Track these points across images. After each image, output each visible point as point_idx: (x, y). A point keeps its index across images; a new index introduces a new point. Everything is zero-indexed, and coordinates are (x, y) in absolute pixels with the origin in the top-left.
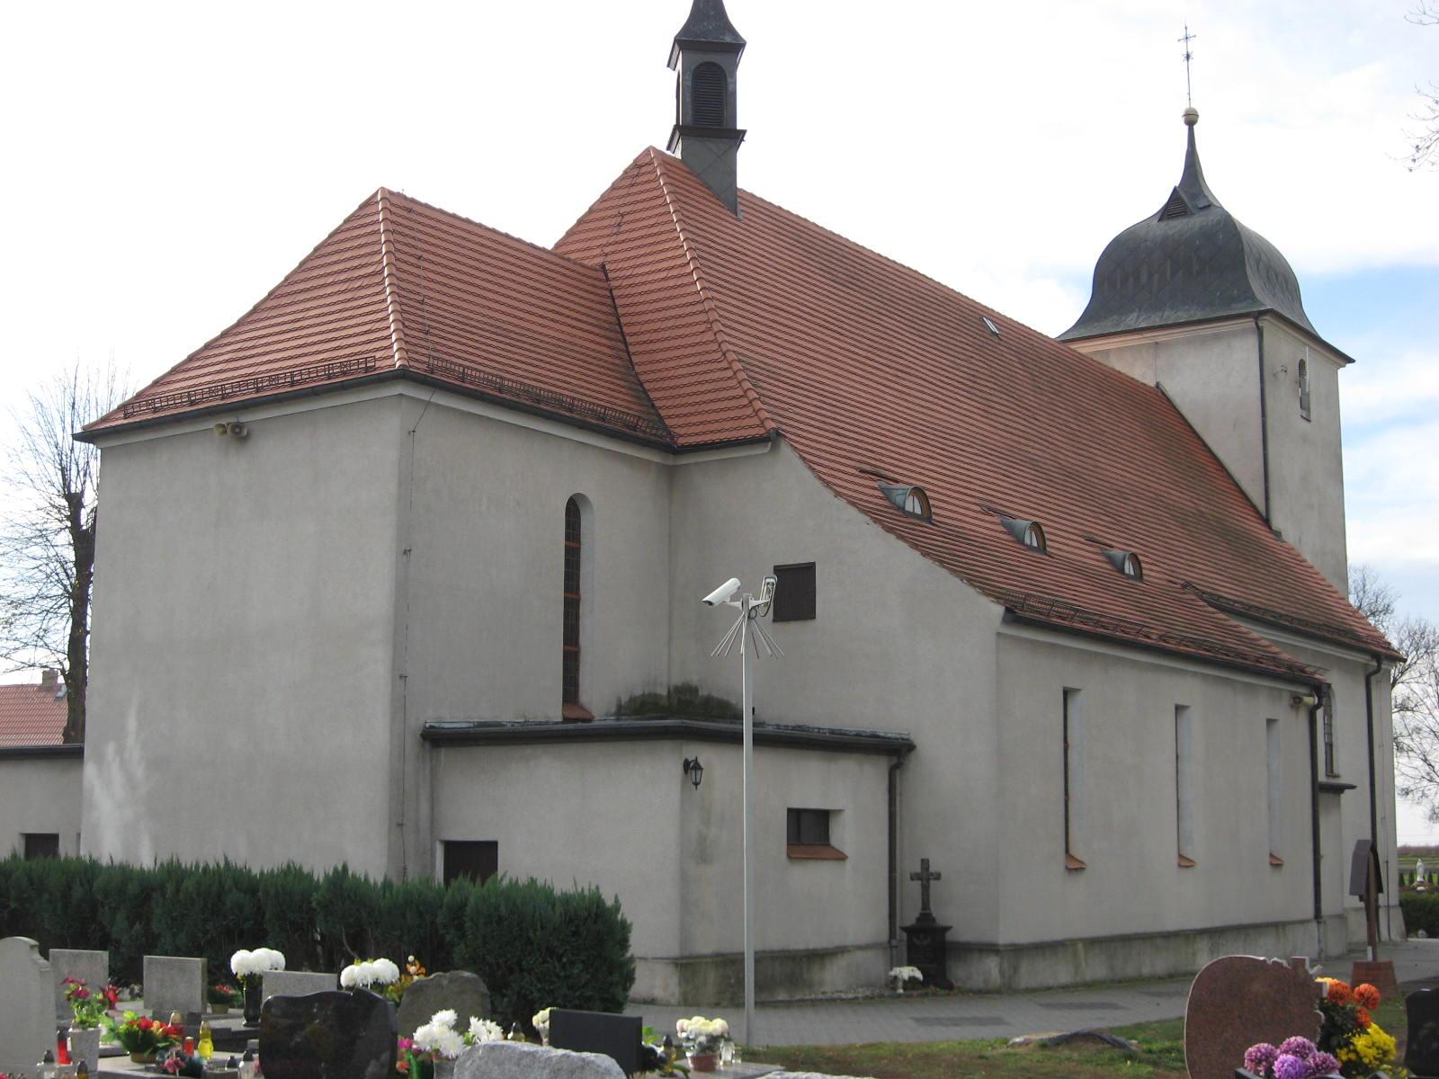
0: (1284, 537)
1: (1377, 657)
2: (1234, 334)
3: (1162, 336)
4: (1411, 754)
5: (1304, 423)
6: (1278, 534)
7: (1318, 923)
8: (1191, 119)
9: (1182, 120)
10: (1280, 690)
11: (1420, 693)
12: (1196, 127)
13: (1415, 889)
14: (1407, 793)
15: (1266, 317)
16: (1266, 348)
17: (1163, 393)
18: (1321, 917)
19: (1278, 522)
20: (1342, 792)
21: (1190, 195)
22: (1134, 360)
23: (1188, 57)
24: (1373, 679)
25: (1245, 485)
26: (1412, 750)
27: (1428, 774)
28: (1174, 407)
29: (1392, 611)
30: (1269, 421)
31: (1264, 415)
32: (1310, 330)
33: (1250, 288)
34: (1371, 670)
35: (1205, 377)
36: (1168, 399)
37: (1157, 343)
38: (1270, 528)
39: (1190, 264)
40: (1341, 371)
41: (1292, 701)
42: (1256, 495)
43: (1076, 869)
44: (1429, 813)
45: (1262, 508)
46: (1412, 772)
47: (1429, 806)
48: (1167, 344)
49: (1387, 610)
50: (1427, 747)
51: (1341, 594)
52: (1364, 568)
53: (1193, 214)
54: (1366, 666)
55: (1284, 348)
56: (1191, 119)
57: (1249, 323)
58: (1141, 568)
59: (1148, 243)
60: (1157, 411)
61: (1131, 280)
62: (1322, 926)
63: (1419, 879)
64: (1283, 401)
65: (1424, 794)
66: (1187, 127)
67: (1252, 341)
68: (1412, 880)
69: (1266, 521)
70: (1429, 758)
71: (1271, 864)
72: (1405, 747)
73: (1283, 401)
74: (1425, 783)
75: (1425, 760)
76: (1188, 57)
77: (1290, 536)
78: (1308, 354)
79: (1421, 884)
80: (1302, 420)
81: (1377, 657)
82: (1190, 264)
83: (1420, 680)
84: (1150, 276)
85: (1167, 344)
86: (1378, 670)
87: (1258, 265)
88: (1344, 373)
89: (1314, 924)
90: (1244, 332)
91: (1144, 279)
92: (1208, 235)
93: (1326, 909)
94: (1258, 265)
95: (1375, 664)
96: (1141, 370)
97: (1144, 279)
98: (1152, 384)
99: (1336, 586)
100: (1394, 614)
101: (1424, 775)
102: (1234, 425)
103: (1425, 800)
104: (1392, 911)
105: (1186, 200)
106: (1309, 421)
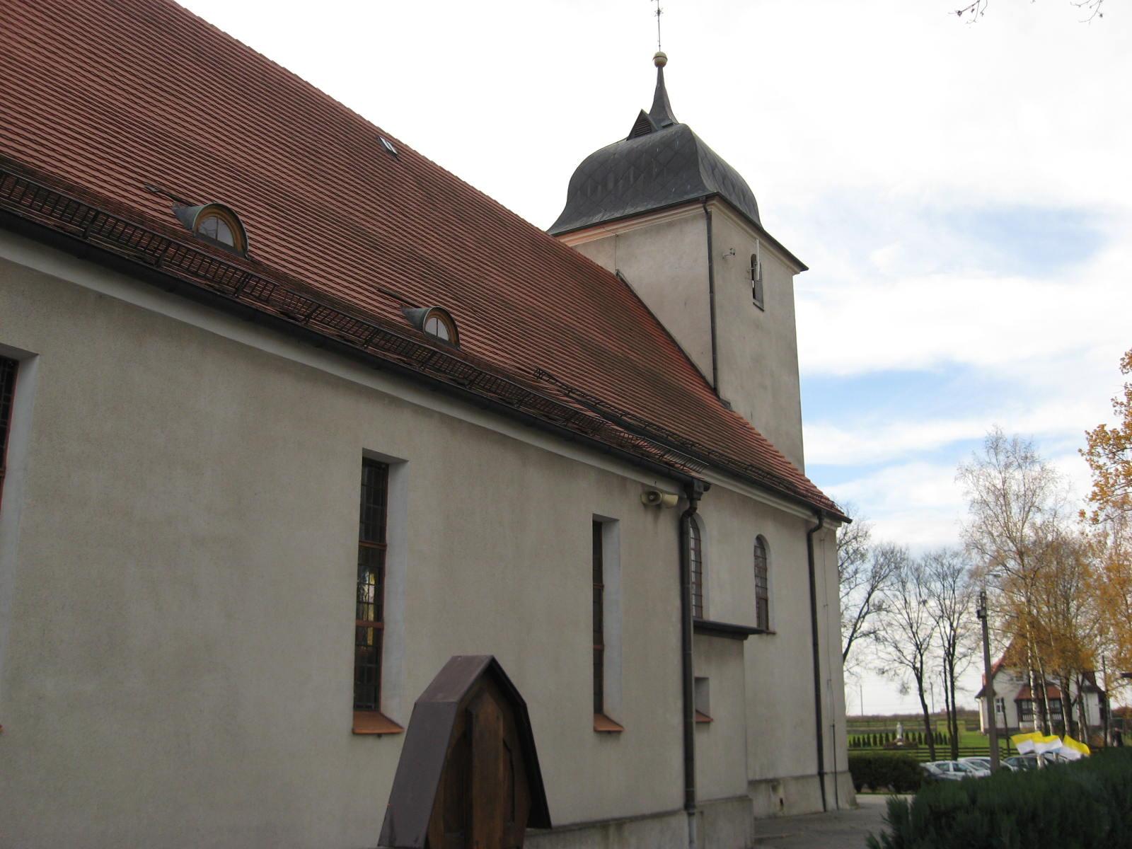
0: (734, 406)
1: (817, 512)
2: (686, 221)
3: (621, 229)
4: (886, 643)
5: (758, 311)
6: (726, 404)
7: (690, 815)
8: (660, 62)
9: (653, 63)
10: (625, 479)
11: (891, 597)
12: (664, 69)
13: (895, 744)
14: (883, 673)
15: (714, 202)
16: (714, 230)
17: (622, 280)
18: (694, 807)
19: (726, 392)
20: (746, 638)
21: (655, 120)
22: (599, 250)
23: (659, 12)
24: (815, 535)
25: (695, 358)
26: (887, 640)
27: (899, 658)
28: (632, 291)
29: (870, 536)
30: (718, 298)
31: (712, 291)
32: (757, 222)
33: (702, 182)
34: (813, 526)
35: (659, 262)
36: (627, 285)
37: (617, 236)
38: (718, 397)
39: (658, 170)
40: (796, 278)
41: (644, 499)
42: (705, 367)
43: (609, 732)
44: (900, 687)
45: (710, 378)
46: (888, 657)
47: (900, 682)
48: (625, 236)
49: (866, 535)
50: (897, 638)
51: (799, 472)
52: (848, 504)
53: (656, 131)
54: (807, 522)
55: (730, 234)
56: (660, 62)
57: (698, 210)
58: (457, 333)
59: (616, 156)
60: (616, 296)
61: (600, 187)
62: (695, 821)
63: (898, 737)
64: (734, 287)
65: (896, 674)
66: (656, 69)
67: (701, 226)
68: (894, 737)
69: (714, 390)
70: (899, 645)
71: (596, 731)
72: (881, 637)
73: (734, 287)
74: (897, 664)
75: (896, 647)
76: (659, 12)
77: (741, 408)
78: (757, 248)
79: (900, 740)
80: (755, 308)
81: (817, 512)
82: (658, 170)
83: (892, 588)
84: (616, 182)
85: (625, 236)
86: (819, 527)
87: (713, 170)
88: (799, 279)
89: (683, 818)
90: (694, 218)
91: (611, 185)
92: (667, 144)
93: (703, 790)
94: (713, 170)
95: (816, 521)
96: (605, 260)
97: (611, 185)
98: (614, 272)
99: (794, 465)
100: (871, 538)
101: (896, 659)
102: (685, 304)
103: (896, 677)
104: (840, 778)
105: (653, 123)
106: (762, 310)
